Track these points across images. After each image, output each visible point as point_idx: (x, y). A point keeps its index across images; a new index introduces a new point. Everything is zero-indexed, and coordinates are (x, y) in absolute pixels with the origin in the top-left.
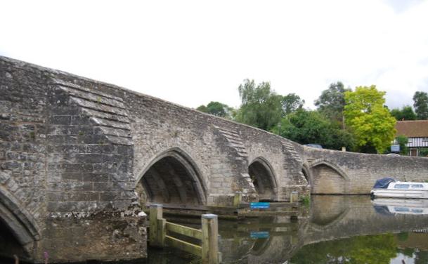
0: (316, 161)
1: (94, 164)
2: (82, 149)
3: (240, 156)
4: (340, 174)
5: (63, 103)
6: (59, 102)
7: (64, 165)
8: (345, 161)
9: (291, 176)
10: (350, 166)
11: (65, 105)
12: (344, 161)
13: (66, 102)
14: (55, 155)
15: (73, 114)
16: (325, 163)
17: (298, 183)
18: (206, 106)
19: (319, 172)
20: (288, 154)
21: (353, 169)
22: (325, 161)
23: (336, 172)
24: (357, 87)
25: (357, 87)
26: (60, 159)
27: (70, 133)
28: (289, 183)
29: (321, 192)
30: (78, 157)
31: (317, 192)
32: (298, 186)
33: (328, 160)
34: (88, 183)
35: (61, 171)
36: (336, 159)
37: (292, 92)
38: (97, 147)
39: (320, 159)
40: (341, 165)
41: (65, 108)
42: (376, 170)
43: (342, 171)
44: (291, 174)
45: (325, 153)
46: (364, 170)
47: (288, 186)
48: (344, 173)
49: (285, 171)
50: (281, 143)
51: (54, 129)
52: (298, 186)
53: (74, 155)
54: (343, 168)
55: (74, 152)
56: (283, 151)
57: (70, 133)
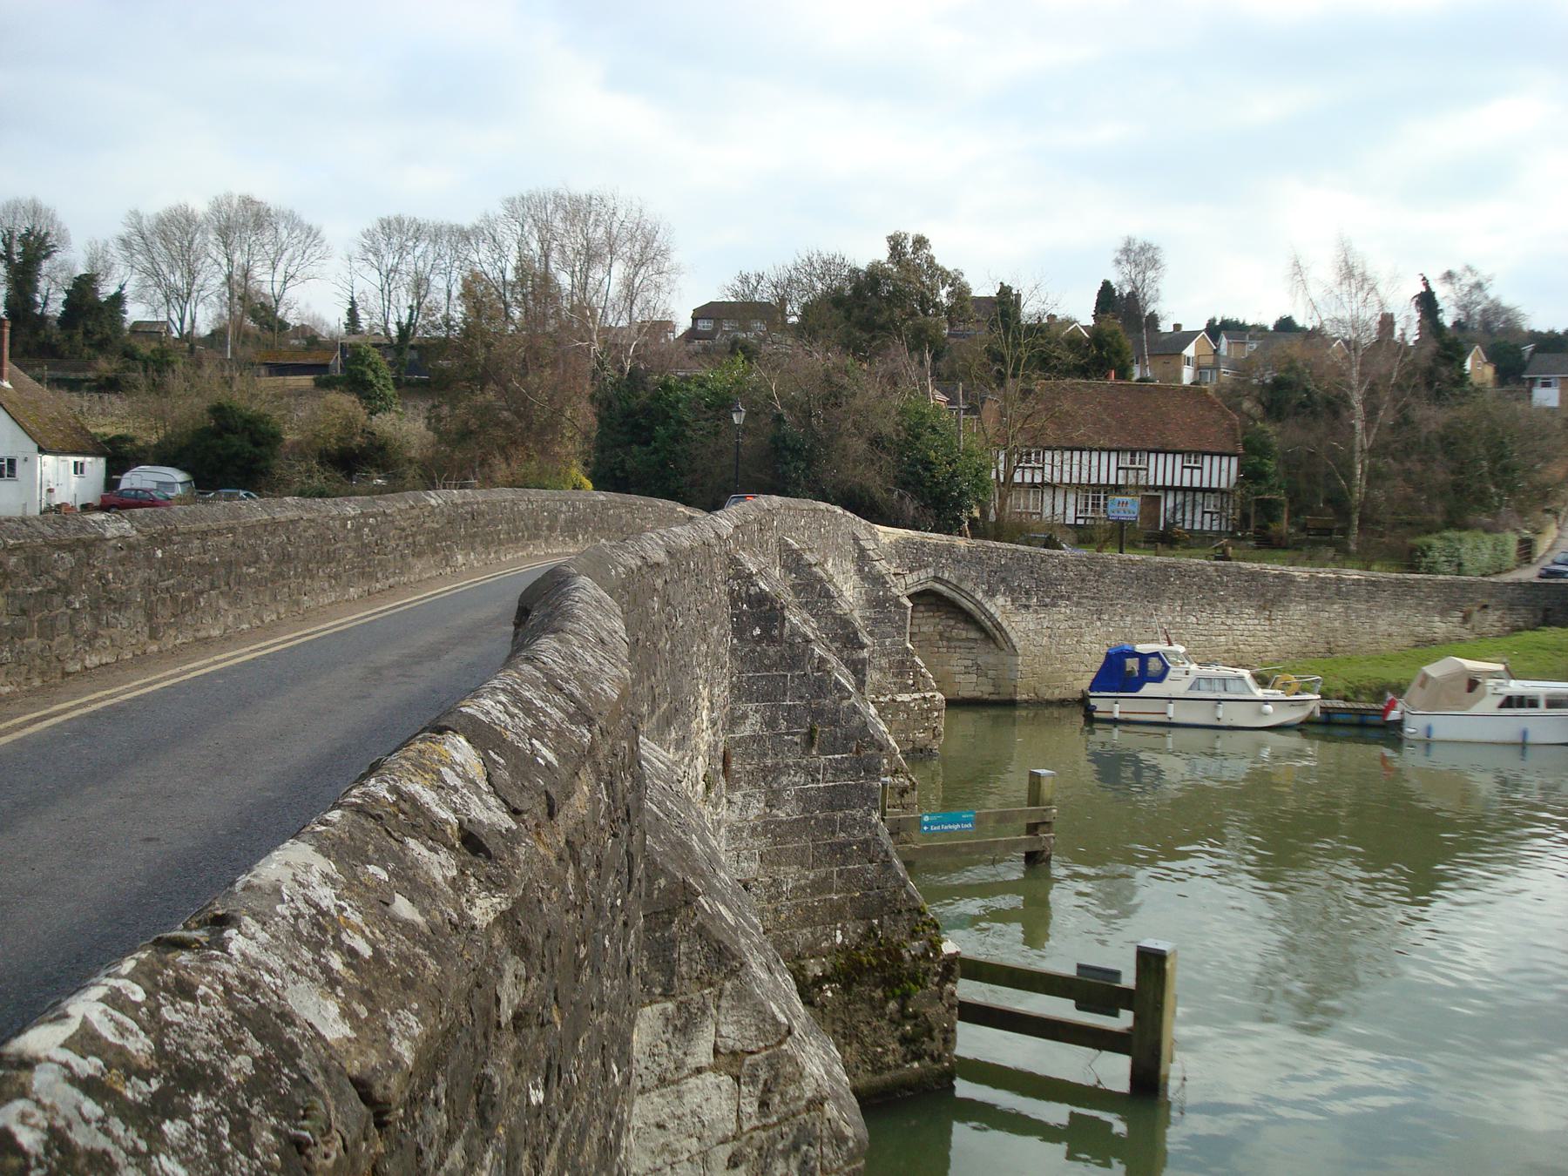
1: (840, 814)
2: (812, 773)
4: (981, 628)
5: (767, 636)
6: (757, 631)
7: (768, 827)
8: (1003, 580)
11: (773, 641)
12: (999, 580)
13: (776, 632)
14: (744, 796)
15: (790, 668)
17: (904, 688)
21: (1027, 607)
22: (936, 579)
23: (968, 618)
24: (1177, 327)
25: (1177, 327)
26: (757, 808)
27: (783, 725)
30: (803, 796)
32: (905, 697)
34: (822, 871)
35: (761, 844)
38: (847, 764)
39: (923, 574)
40: (991, 593)
41: (771, 651)
42: (1100, 612)
43: (991, 617)
45: (938, 550)
46: (1064, 609)
48: (998, 626)
51: (745, 716)
52: (905, 697)
53: (792, 791)
54: (998, 607)
55: (793, 782)
56: (860, 571)
57: (783, 725)
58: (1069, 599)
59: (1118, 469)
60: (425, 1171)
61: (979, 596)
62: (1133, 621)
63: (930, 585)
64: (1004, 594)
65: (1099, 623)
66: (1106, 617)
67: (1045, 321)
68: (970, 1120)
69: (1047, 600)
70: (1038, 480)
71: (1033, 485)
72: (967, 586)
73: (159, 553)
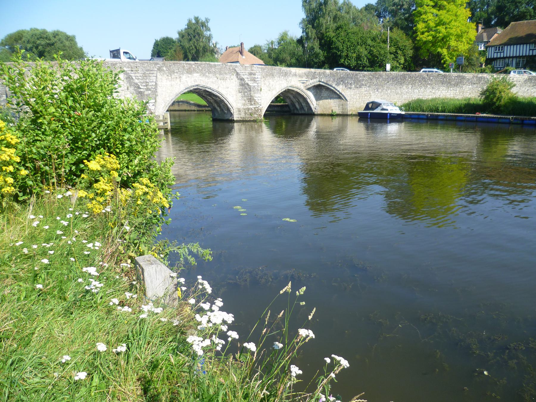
0: (311, 81)
3: (141, 88)
8: (342, 81)
9: (245, 98)
10: (348, 86)
12: (342, 80)
16: (321, 83)
17: (251, 105)
18: (175, 36)
19: (321, 92)
20: (242, 79)
21: (350, 88)
22: (320, 81)
28: (244, 105)
29: (322, 113)
31: (319, 113)
32: (251, 107)
33: (322, 80)
36: (332, 80)
37: (164, 35)
39: (315, 80)
40: (338, 84)
44: (245, 97)
47: (243, 107)
49: (240, 94)
50: (235, 70)
52: (251, 107)
54: (340, 88)
56: (237, 77)
58: (366, 85)
59: (530, 50)
60: (2, 76)
61: (334, 85)
62: (391, 92)
63: (318, 83)
64: (342, 84)
65: (377, 92)
66: (380, 90)
67: (194, 21)
68: (353, 397)
69: (358, 86)
70: (502, 56)
71: (500, 58)
72: (330, 83)
73: (237, 277)
